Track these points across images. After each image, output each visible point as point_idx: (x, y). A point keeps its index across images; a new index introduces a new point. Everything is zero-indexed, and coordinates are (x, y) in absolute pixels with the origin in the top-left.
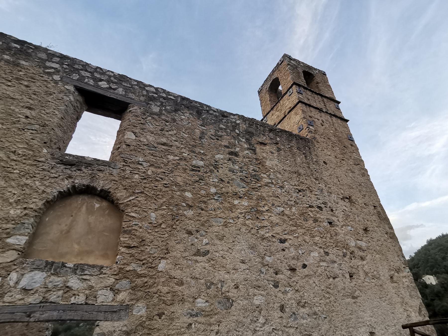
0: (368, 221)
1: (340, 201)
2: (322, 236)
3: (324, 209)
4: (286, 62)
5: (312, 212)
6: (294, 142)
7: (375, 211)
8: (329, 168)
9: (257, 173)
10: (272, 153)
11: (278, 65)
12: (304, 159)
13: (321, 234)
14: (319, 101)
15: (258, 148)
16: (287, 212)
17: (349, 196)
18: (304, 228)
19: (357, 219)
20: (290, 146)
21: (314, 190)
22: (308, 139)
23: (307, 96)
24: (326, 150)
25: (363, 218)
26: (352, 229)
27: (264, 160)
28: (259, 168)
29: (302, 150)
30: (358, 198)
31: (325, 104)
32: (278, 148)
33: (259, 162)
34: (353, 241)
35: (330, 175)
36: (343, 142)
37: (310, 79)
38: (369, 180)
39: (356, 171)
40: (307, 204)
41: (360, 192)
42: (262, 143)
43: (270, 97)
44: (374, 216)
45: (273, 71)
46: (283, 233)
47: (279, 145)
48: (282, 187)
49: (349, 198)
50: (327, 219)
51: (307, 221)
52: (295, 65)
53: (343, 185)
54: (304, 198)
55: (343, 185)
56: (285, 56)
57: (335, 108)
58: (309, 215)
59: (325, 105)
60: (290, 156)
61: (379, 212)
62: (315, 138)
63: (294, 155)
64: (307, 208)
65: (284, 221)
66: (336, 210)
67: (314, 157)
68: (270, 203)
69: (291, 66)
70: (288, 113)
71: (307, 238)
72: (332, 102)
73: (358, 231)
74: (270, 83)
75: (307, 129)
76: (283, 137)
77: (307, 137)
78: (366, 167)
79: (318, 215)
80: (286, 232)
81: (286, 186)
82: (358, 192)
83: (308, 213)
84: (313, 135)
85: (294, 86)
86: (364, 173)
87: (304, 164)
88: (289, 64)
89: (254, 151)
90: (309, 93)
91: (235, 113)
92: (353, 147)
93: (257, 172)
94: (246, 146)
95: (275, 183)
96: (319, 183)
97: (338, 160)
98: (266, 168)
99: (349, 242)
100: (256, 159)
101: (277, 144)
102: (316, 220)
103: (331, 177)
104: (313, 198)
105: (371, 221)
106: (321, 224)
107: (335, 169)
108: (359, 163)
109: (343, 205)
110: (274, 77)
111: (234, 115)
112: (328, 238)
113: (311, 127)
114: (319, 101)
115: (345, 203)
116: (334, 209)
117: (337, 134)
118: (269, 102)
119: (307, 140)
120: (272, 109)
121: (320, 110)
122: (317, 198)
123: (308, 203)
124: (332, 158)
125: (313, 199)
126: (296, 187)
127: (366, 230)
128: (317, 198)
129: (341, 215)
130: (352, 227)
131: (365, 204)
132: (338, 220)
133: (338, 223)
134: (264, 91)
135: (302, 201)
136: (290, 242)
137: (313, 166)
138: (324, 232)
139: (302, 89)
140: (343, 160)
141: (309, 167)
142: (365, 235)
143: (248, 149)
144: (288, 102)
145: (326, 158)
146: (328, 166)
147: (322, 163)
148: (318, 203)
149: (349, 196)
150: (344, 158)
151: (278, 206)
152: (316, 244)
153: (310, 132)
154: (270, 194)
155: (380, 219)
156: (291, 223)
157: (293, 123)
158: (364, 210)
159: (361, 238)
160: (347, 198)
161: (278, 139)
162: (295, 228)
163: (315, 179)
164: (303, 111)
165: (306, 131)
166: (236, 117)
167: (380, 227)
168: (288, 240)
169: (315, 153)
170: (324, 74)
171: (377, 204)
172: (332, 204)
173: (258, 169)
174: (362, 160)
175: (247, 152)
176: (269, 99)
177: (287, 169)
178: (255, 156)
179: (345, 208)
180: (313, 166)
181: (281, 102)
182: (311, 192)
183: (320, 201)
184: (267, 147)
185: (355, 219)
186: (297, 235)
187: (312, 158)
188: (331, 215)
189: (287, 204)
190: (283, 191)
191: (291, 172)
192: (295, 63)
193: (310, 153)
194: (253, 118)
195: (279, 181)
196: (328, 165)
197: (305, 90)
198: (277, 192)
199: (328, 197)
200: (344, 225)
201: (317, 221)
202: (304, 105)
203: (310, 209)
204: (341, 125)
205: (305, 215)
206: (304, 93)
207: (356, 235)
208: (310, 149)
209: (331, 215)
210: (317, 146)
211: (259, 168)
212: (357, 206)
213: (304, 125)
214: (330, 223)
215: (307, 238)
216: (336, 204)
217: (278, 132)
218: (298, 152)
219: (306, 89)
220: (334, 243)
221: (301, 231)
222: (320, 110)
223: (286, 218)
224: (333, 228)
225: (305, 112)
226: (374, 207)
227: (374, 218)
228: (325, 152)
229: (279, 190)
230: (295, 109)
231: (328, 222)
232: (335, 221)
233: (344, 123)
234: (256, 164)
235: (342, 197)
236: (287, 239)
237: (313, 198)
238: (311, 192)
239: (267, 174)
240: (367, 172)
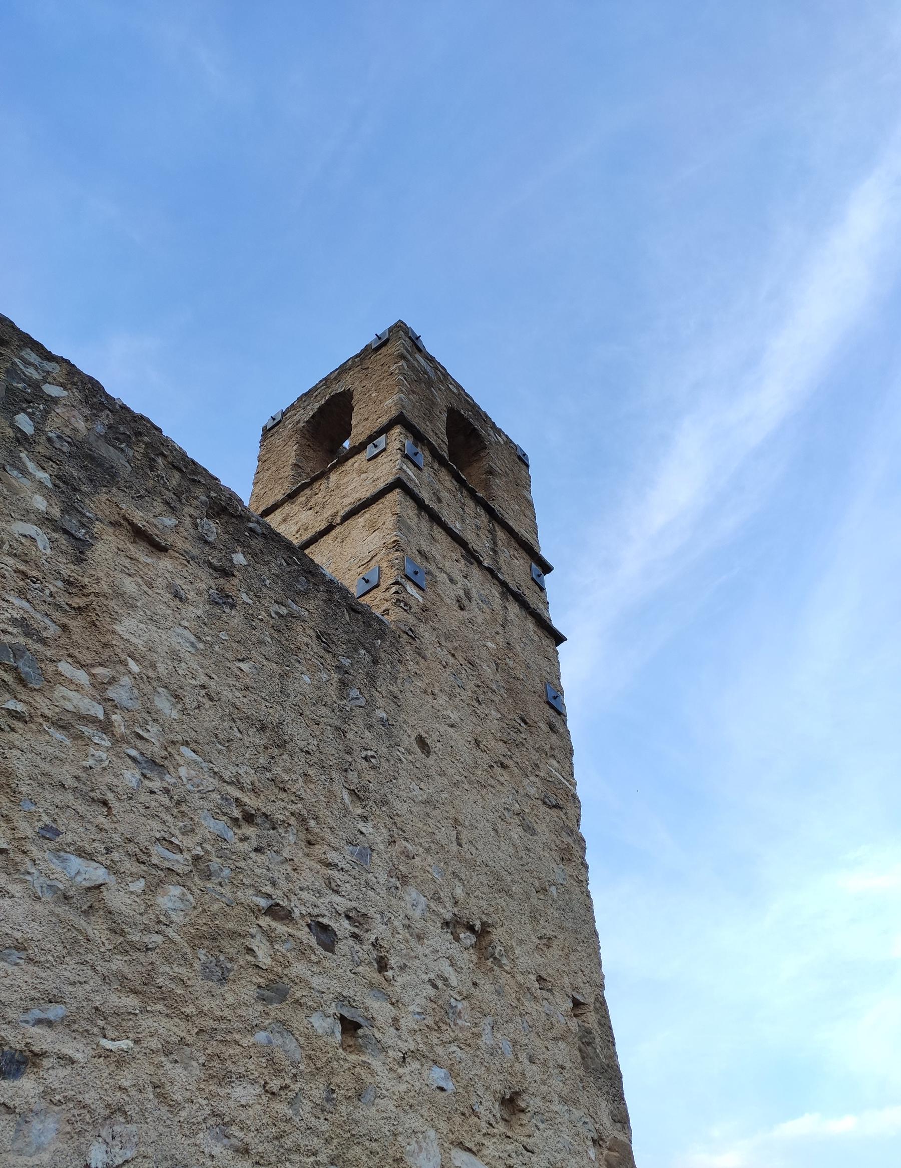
0: (532, 1061)
1: (434, 928)
2: (275, 1085)
3: (345, 946)
4: (393, 349)
5: (270, 937)
6: (311, 605)
7: (573, 1024)
8: (432, 771)
9: (39, 647)
10: (177, 595)
11: (368, 352)
12: (332, 692)
13: (278, 1072)
14: (478, 528)
15: (108, 547)
16: (118, 899)
17: (484, 924)
18: (187, 1018)
19: (487, 1040)
20: (284, 611)
21: (328, 836)
22: (381, 622)
23: (433, 483)
24: (442, 699)
25: (515, 1043)
26: (450, 1086)
27: (112, 604)
28: (64, 627)
29: (341, 649)
30: (521, 942)
31: (495, 544)
32: (220, 590)
33: (77, 601)
34: (435, 1149)
35: (426, 802)
36: (524, 701)
37: (464, 448)
38: (583, 883)
39: (541, 828)
40: (259, 893)
41: (534, 918)
42: (139, 534)
43: (301, 454)
44: (562, 1045)
45: (343, 369)
46: (36, 1013)
47: (235, 581)
48: (154, 765)
49: (482, 933)
50: (341, 999)
51: (223, 980)
52: (426, 373)
53: (472, 865)
54: (259, 858)
55: (472, 865)
56: (400, 328)
57: (528, 579)
58: (250, 951)
59: (495, 551)
60: (264, 650)
61: (589, 1032)
62: (412, 635)
63: (287, 653)
64: (257, 911)
65: (77, 944)
66: (403, 967)
67: (381, 702)
68: (30, 817)
69: (411, 367)
70: (345, 518)
71: (181, 1077)
72: (524, 554)
73: (474, 1099)
74: (317, 406)
75: (393, 590)
76: (267, 563)
77: (385, 618)
78: (585, 829)
79: (299, 968)
80: (55, 1012)
81: (183, 771)
82: (525, 919)
83: (248, 942)
84: (412, 620)
85: (397, 430)
86: (568, 849)
87: (324, 711)
88: (402, 357)
89: (80, 550)
90: (449, 482)
91: (56, 352)
92: (554, 737)
93: (44, 641)
94: (40, 503)
95: (121, 729)
96: (365, 819)
97: (485, 759)
98: (106, 645)
99: (414, 1146)
100: (68, 582)
101: (225, 573)
102: (274, 991)
103: (429, 809)
104: (307, 874)
105: (545, 1063)
106: (298, 1020)
107: (456, 784)
108: (562, 801)
109: (443, 956)
110: (339, 388)
111: (49, 357)
112: (307, 1105)
113: (411, 589)
114: (478, 528)
115: (454, 950)
116: (393, 961)
117: (511, 663)
118: (288, 471)
119: (376, 626)
120: (291, 497)
121: (472, 556)
122: (329, 882)
123: (269, 889)
124: (460, 740)
125: (307, 878)
126: (237, 794)
127: (511, 1103)
128: (329, 882)
129: (417, 1000)
130: (453, 1074)
131: (540, 979)
132: (396, 1020)
133: (389, 1037)
134: (286, 430)
135: (238, 870)
136: (56, 1076)
137: (358, 734)
138: (295, 1064)
139: (427, 453)
140: (503, 766)
141: (341, 732)
142: (501, 1128)
143: (46, 521)
144: (355, 480)
145: (435, 731)
146: (431, 761)
147: (408, 741)
148: (326, 906)
149: (484, 924)
150: (506, 762)
151: (81, 853)
152: (222, 1124)
153: (402, 603)
154: (65, 773)
155: (587, 1068)
156: (118, 963)
157: (348, 558)
158: (529, 1005)
159: (478, 1137)
160: (471, 928)
161: (239, 558)
162: (132, 1002)
163: (352, 792)
164: (400, 522)
165: (388, 595)
166: (49, 366)
167: (576, 1102)
168: (46, 1063)
169: (394, 689)
170: (522, 460)
171: (587, 995)
172: (395, 932)
173: (52, 631)
174: (575, 799)
175: (31, 529)
176: (292, 460)
177: (227, 694)
178: (67, 569)
179: (449, 972)
180: (358, 734)
181: (333, 477)
182: (310, 843)
183: (337, 899)
184: (165, 564)
185: (478, 1036)
186: (125, 1044)
187: (371, 704)
188: (371, 985)
189: (142, 858)
190: (156, 785)
191: (236, 714)
192: (428, 369)
193: (372, 679)
194: (142, 417)
195: (154, 729)
196: (433, 757)
197: (436, 466)
198: (109, 778)
199: (383, 893)
200: (414, 1054)
201: (282, 995)
202: (413, 504)
203: (265, 921)
204: (532, 640)
205: (224, 943)
206: (427, 471)
207: (458, 1119)
208: (375, 662)
209: (371, 985)
210: (412, 666)
211: (64, 627)
212: (504, 978)
213: (386, 571)
214: (350, 1027)
215: (181, 1077)
216: (413, 942)
217: (251, 530)
218: (318, 649)
219: (442, 461)
220: (328, 1141)
221: (161, 1026)
222: (472, 556)
223: (97, 929)
224: (353, 1058)
225: (409, 528)
226: (577, 1004)
227: (564, 1053)
228: (432, 701)
229: (131, 776)
230: (375, 508)
231: (342, 1019)
232: (380, 1021)
233: (546, 642)
234: (58, 607)
235: (448, 916)
236: (43, 1054)
237: (307, 874)
238: (310, 843)
239: (98, 670)
240: (584, 849)
